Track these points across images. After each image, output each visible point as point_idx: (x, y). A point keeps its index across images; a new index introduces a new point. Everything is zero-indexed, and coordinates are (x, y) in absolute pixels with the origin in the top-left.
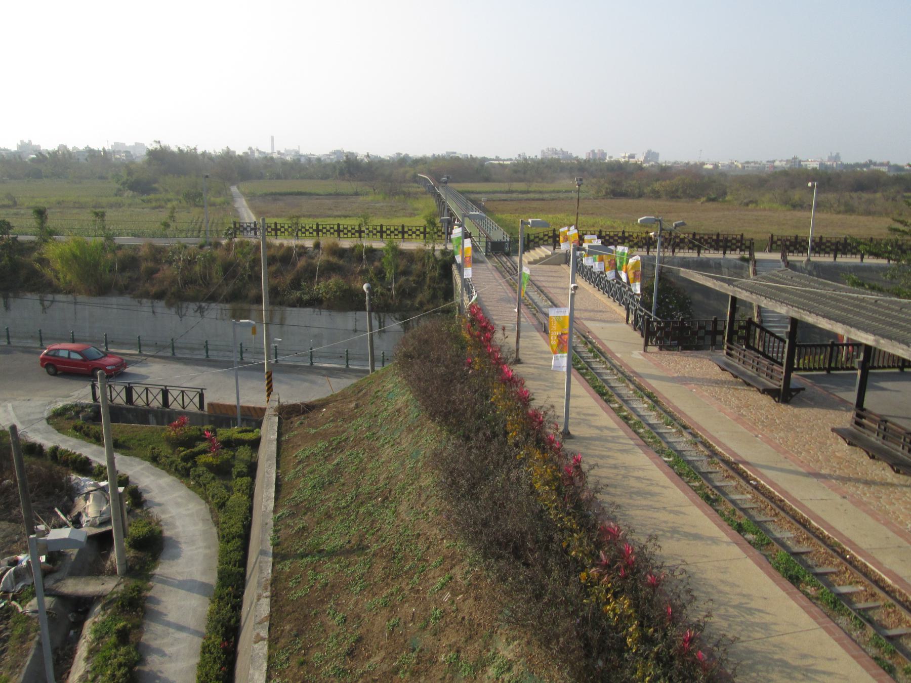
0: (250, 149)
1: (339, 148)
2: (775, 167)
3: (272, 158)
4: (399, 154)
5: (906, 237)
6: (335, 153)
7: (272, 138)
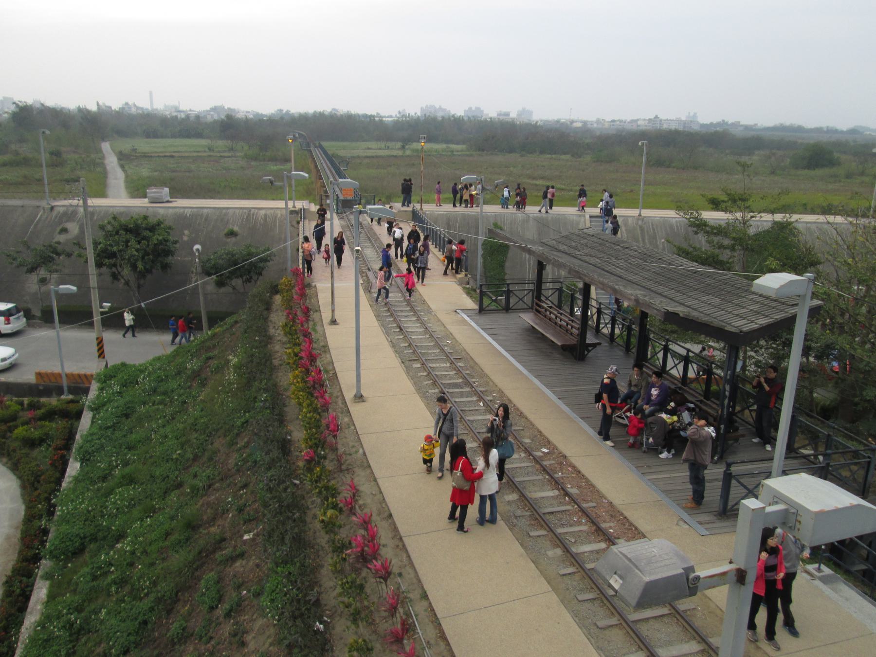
0: (127, 104)
1: (219, 104)
2: (638, 126)
4: (281, 110)
5: (262, 633)
6: (214, 109)
7: (151, 93)
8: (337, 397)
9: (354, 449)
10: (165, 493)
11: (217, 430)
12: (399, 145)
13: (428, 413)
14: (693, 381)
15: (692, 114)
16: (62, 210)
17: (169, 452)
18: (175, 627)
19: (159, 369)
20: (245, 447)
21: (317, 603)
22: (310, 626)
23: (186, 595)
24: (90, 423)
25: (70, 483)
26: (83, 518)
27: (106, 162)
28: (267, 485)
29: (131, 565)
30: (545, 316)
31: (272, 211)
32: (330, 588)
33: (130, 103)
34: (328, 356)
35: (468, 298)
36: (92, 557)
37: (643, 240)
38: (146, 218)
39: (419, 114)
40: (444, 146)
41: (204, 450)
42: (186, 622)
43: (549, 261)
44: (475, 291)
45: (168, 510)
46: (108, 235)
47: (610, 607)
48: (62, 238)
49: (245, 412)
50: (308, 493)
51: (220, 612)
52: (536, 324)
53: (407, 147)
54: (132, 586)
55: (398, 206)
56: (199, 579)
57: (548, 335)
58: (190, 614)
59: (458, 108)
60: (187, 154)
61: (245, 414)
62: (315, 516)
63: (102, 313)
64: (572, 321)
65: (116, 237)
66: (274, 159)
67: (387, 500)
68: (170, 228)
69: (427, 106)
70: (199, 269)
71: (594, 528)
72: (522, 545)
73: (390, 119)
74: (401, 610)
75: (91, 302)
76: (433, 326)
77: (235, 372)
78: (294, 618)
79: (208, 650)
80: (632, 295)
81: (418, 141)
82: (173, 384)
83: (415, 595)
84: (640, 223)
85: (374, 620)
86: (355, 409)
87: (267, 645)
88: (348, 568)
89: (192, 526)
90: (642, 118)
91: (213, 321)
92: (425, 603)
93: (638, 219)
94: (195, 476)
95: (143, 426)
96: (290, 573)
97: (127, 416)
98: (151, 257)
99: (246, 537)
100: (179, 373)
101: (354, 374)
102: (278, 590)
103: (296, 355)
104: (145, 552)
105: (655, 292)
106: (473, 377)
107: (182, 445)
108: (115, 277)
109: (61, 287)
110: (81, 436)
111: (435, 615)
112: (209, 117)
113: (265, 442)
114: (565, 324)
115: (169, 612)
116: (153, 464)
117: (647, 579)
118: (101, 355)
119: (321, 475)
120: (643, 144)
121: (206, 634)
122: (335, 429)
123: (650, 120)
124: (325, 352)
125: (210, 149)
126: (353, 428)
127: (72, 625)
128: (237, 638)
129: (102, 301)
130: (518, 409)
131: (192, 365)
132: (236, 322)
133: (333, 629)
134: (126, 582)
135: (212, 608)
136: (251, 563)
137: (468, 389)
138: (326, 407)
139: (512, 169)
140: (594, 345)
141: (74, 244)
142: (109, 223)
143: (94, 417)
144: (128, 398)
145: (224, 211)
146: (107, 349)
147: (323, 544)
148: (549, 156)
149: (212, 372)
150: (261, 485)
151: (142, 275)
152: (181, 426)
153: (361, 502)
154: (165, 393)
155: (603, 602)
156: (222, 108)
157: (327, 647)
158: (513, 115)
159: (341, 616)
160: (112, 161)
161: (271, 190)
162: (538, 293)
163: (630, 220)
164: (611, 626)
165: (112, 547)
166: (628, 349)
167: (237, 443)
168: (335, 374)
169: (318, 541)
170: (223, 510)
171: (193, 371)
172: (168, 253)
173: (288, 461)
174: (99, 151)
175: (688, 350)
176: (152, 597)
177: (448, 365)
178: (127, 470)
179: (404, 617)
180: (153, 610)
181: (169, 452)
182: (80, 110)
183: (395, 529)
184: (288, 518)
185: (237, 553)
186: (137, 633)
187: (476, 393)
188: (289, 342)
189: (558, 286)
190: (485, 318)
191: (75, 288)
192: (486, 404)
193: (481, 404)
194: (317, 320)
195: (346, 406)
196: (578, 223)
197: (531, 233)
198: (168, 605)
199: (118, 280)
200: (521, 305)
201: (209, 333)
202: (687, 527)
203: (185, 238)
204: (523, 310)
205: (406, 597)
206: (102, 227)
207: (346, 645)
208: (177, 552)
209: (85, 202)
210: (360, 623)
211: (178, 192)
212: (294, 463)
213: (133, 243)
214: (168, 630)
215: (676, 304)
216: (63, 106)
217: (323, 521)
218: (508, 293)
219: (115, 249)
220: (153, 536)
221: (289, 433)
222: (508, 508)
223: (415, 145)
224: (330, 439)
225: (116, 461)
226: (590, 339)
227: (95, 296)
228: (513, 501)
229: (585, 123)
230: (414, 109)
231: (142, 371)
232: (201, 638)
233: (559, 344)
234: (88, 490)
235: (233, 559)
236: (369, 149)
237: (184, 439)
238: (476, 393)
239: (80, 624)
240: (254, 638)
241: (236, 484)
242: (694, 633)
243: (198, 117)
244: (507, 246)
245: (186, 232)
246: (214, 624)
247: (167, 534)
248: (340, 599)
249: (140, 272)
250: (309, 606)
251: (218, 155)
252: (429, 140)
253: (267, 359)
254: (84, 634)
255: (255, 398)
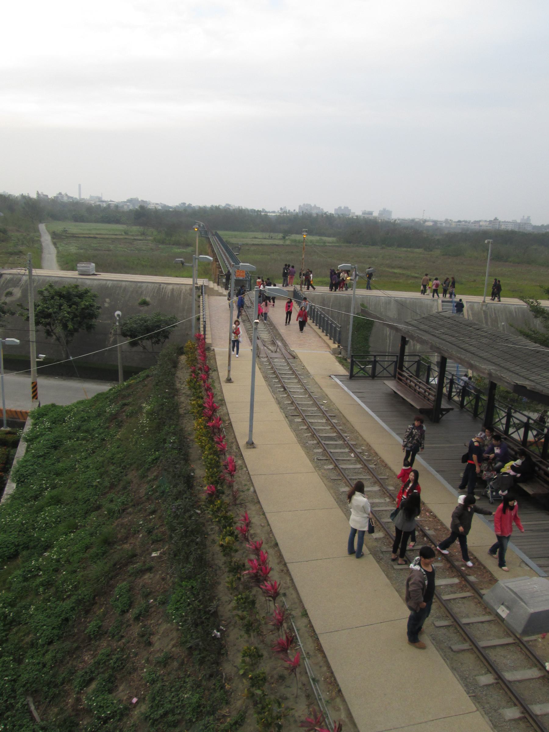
0: (60, 194)
1: (134, 197)
2: (481, 226)
3: (333, 216)
4: (184, 204)
6: (130, 201)
7: (80, 186)
8: (232, 443)
9: (246, 487)
10: (86, 513)
11: (131, 465)
12: (281, 235)
13: (308, 461)
14: (531, 444)
15: (526, 217)
16: (9, 277)
17: (90, 480)
18: (91, 626)
19: (83, 411)
20: (154, 480)
21: (215, 614)
22: (209, 633)
23: (102, 599)
24: (25, 451)
25: (8, 499)
26: (18, 529)
27: (42, 239)
28: (175, 512)
29: (56, 571)
30: (406, 384)
31: (178, 286)
32: (227, 603)
33: (63, 193)
34: (224, 408)
35: (340, 366)
36: (23, 562)
37: (487, 323)
38: (77, 287)
39: (297, 211)
40: (318, 238)
41: (120, 480)
42: (102, 621)
43: (412, 337)
44: (346, 360)
45: (88, 528)
46: (45, 300)
47: (462, 633)
48: (8, 300)
49: (155, 451)
50: (208, 521)
51: (130, 615)
52: (398, 390)
53: (287, 238)
54: (57, 588)
55: (279, 286)
56: (113, 587)
57: (408, 400)
58: (104, 614)
59: (329, 207)
60: (107, 236)
61: (155, 453)
62: (214, 541)
63: (39, 364)
64: (430, 389)
65: (52, 301)
66: (177, 244)
67: (274, 531)
68: (95, 296)
69: (304, 205)
70: (119, 331)
71: (448, 565)
72: (387, 575)
73: (273, 214)
74: (285, 625)
75: (29, 353)
76: (312, 388)
77: (148, 418)
78: (197, 625)
79: (119, 647)
80: (485, 369)
81: (300, 233)
82: (94, 424)
83: (297, 613)
84: (484, 308)
85: (262, 632)
86: (247, 454)
87: (170, 647)
88: (241, 587)
89: (108, 542)
90: (484, 219)
91: (129, 373)
92: (305, 620)
93: (482, 305)
94: (112, 501)
95: (69, 457)
96: (193, 587)
97: (55, 448)
98: (79, 319)
99: (154, 554)
100: (99, 415)
101: (248, 424)
102: (182, 601)
103: (200, 406)
104: (68, 561)
105: (503, 367)
106: (345, 432)
107: (101, 475)
108: (49, 333)
109: (7, 339)
110: (18, 462)
111: (314, 631)
112: (125, 207)
113: (174, 477)
114: (423, 391)
115: (87, 612)
116: (76, 489)
117: (532, 611)
118: (35, 396)
119: (221, 507)
120: (489, 242)
121: (118, 633)
122: (232, 470)
123: (490, 221)
124: (222, 405)
125: (126, 233)
126: (245, 469)
127: (6, 617)
128: (145, 638)
129: (38, 353)
130: (383, 461)
131: (111, 409)
132: (148, 376)
133: (228, 636)
134: (52, 585)
135: (124, 612)
136: (158, 576)
137: (341, 442)
138: (223, 451)
139: (374, 259)
140: (448, 410)
141: (18, 305)
142: (46, 290)
143: (28, 447)
144: (56, 434)
145: (139, 284)
146: (39, 391)
147: (220, 565)
148: (405, 249)
149: (127, 416)
150: (169, 512)
151: (71, 333)
152: (100, 459)
153: (252, 532)
154: (86, 431)
155: (456, 629)
156: (136, 200)
157: (223, 651)
158: (376, 214)
159: (234, 626)
160: (46, 239)
161: (179, 269)
162: (400, 364)
163: (475, 305)
164: (464, 650)
165: (41, 555)
166: (476, 415)
167: (147, 476)
168: (230, 424)
169: (216, 562)
170: (135, 531)
171: (112, 414)
172: (93, 316)
173: (191, 494)
174: (37, 230)
175: (529, 418)
176: (73, 598)
177: (324, 421)
178: (55, 492)
179: (288, 631)
180: (74, 609)
181: (90, 480)
182: (23, 197)
183: (281, 556)
184: (192, 541)
185: (146, 567)
186: (60, 628)
187: (348, 446)
188: (194, 395)
189: (417, 358)
190: (354, 384)
191: (18, 341)
192: (356, 455)
193: (352, 455)
194: (215, 378)
195: (240, 451)
196: (431, 307)
197: (392, 313)
198: (86, 607)
199: (52, 336)
200: (385, 373)
201: (125, 383)
202: (528, 568)
203: (106, 305)
204: (387, 378)
205: (290, 614)
206: (41, 293)
207: (239, 651)
208: (95, 562)
209: (30, 272)
210: (252, 634)
211: (102, 267)
212: (196, 496)
213: (65, 307)
214: (86, 627)
215: (522, 378)
216: (11, 193)
217: (222, 546)
218: (374, 363)
219: (51, 310)
220: (75, 549)
221: (193, 470)
222: (375, 544)
223: (298, 237)
224: (228, 477)
225: (46, 485)
226: (444, 405)
227: (33, 348)
228: (380, 539)
229: (435, 222)
230: (293, 205)
231: (68, 412)
232: (113, 636)
233: (418, 408)
234: (23, 506)
235: (142, 572)
236: (256, 238)
237: (103, 470)
238: (348, 446)
239: (12, 617)
240: (159, 639)
241: (146, 510)
242: (534, 660)
243: (117, 206)
244: (371, 323)
245: (107, 300)
246: (125, 626)
247: (87, 548)
248: (235, 612)
249: (69, 331)
250: (208, 616)
251: (132, 238)
252: (310, 233)
253: (176, 407)
254: (15, 626)
255: (165, 440)
